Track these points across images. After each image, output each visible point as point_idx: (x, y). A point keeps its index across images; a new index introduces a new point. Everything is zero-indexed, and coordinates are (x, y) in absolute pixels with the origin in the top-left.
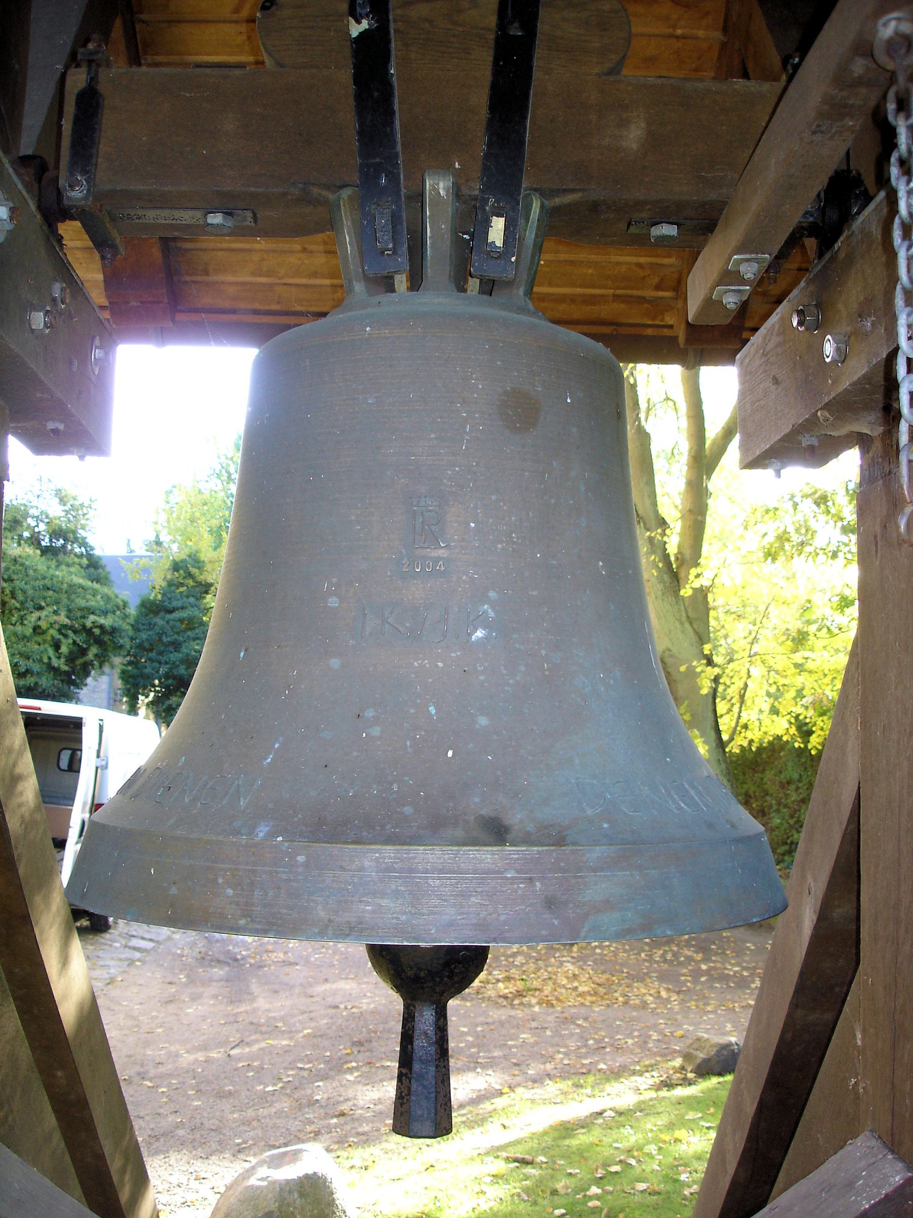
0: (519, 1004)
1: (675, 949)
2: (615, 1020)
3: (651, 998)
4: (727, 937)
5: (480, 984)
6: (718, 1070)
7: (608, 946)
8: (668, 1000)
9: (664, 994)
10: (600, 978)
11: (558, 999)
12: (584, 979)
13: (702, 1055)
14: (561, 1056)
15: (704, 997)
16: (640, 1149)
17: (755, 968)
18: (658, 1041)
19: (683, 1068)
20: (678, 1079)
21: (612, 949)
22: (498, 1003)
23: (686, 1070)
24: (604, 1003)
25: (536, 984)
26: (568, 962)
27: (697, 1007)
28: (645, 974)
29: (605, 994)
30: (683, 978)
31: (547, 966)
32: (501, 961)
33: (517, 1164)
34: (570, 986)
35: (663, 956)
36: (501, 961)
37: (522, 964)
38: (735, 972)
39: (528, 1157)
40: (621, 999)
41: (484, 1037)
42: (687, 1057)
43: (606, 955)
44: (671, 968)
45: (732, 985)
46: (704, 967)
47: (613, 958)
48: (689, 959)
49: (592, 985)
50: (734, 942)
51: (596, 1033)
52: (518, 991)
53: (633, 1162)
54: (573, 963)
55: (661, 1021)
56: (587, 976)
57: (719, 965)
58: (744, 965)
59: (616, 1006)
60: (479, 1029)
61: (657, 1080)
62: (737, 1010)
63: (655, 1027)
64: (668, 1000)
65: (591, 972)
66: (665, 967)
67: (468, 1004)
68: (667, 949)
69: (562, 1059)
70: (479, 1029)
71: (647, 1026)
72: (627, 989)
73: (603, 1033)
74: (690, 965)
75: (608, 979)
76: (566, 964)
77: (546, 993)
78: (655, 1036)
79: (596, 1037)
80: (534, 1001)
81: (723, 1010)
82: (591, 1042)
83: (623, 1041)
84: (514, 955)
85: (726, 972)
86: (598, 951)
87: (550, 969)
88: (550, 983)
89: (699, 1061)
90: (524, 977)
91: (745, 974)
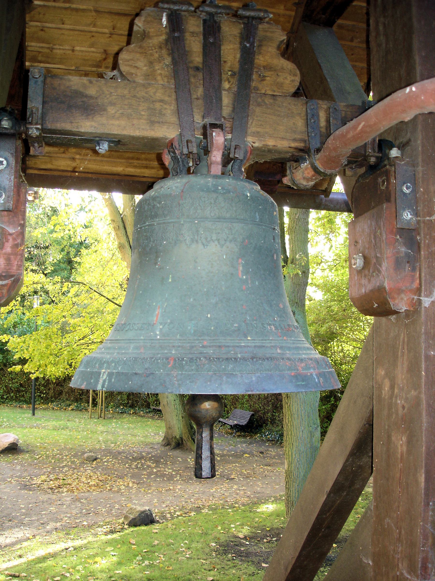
0: (57, 492)
1: (143, 462)
2: (101, 499)
3: (124, 487)
4: (170, 455)
5: (41, 482)
6: (139, 524)
7: (111, 461)
8: (132, 488)
9: (131, 485)
10: (102, 477)
11: (77, 489)
12: (94, 478)
13: (132, 517)
14: (66, 518)
15: (150, 486)
16: (74, 568)
17: (179, 470)
18: (118, 509)
19: (123, 523)
20: (120, 529)
21: (113, 462)
22: (47, 492)
23: (125, 524)
24: (100, 490)
25: (69, 481)
26: (89, 469)
27: (144, 491)
28: (125, 475)
29: (102, 486)
30: (143, 476)
31: (78, 472)
32: (56, 470)
33: (11, 577)
34: (86, 482)
35: (136, 466)
36: (56, 470)
37: (66, 471)
38: (169, 473)
39: (17, 574)
40: (108, 488)
41: (31, 510)
42: (126, 517)
43: (109, 466)
44: (139, 471)
45: (165, 479)
46: (155, 470)
47: (112, 467)
48: (149, 466)
49: (97, 481)
50: (173, 458)
51: (88, 506)
52: (59, 485)
53: (68, 575)
54: (92, 470)
55: (123, 499)
56: (96, 476)
57: (162, 469)
58: (175, 469)
59: (105, 491)
60: (30, 506)
61: (108, 530)
62: (163, 492)
63: (118, 502)
64: (132, 488)
65: (99, 475)
66: (136, 471)
67: (31, 493)
68: (139, 462)
69: (67, 520)
70: (30, 506)
71: (115, 502)
72: (114, 483)
73: (92, 506)
74: (149, 469)
75: (106, 478)
76: (88, 471)
77: (73, 485)
78: (117, 506)
79: (88, 508)
80: (65, 490)
81: (156, 492)
82: (84, 511)
83: (100, 510)
84: (63, 467)
85: (165, 472)
86: (106, 464)
87: (79, 474)
88: (77, 480)
89: (130, 519)
90: (65, 478)
91: (174, 473)
